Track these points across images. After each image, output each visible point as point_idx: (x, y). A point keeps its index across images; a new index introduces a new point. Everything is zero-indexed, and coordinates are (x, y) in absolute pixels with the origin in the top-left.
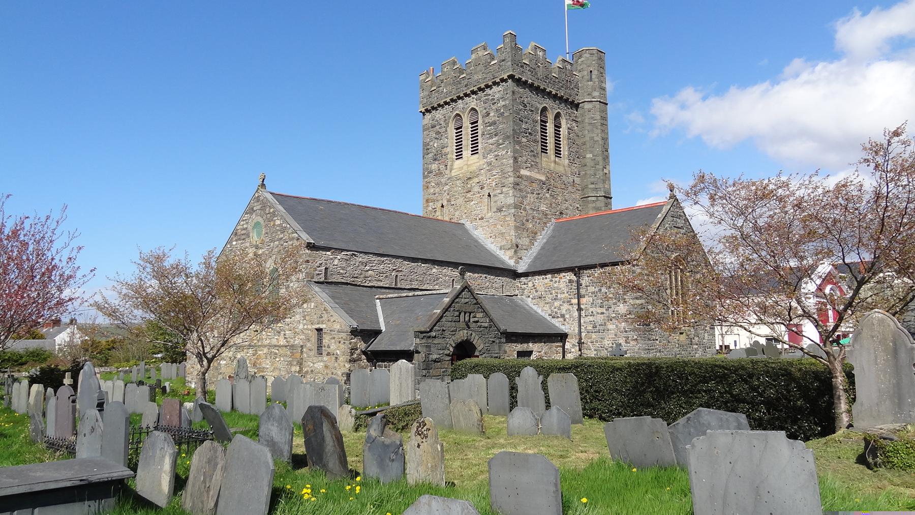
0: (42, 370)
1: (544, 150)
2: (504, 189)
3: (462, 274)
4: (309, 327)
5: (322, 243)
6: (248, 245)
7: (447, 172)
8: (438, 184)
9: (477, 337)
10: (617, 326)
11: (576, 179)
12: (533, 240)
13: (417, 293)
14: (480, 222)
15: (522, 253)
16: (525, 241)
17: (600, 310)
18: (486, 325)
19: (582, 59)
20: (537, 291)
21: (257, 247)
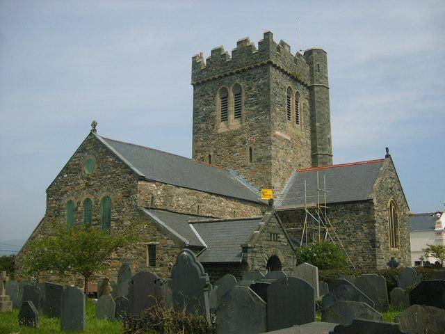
0: (437, 262)
4: (142, 243)
5: (148, 177)
6: (79, 177)
8: (205, 140)
13: (215, 220)
18: (286, 244)
21: (88, 179)
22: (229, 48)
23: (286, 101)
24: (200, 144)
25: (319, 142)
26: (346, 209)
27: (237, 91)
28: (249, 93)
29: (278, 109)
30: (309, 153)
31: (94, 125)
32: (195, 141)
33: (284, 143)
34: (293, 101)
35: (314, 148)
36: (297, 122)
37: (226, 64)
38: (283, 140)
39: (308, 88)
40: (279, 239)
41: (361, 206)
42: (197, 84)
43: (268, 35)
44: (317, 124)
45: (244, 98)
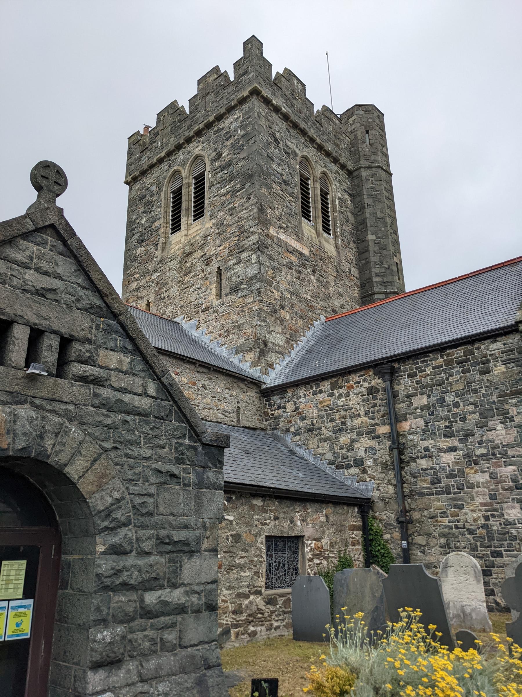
1: (306, 214)
2: (244, 256)
3: (107, 296)
7: (158, 253)
9: (90, 450)
10: (493, 476)
11: (352, 269)
12: (293, 338)
14: (202, 316)
15: (271, 357)
16: (277, 339)
17: (445, 443)
18: (145, 403)
19: (353, 118)
20: (303, 419)
24: (134, 285)
26: (448, 363)
39: (350, 173)
43: (253, 45)
44: (371, 237)
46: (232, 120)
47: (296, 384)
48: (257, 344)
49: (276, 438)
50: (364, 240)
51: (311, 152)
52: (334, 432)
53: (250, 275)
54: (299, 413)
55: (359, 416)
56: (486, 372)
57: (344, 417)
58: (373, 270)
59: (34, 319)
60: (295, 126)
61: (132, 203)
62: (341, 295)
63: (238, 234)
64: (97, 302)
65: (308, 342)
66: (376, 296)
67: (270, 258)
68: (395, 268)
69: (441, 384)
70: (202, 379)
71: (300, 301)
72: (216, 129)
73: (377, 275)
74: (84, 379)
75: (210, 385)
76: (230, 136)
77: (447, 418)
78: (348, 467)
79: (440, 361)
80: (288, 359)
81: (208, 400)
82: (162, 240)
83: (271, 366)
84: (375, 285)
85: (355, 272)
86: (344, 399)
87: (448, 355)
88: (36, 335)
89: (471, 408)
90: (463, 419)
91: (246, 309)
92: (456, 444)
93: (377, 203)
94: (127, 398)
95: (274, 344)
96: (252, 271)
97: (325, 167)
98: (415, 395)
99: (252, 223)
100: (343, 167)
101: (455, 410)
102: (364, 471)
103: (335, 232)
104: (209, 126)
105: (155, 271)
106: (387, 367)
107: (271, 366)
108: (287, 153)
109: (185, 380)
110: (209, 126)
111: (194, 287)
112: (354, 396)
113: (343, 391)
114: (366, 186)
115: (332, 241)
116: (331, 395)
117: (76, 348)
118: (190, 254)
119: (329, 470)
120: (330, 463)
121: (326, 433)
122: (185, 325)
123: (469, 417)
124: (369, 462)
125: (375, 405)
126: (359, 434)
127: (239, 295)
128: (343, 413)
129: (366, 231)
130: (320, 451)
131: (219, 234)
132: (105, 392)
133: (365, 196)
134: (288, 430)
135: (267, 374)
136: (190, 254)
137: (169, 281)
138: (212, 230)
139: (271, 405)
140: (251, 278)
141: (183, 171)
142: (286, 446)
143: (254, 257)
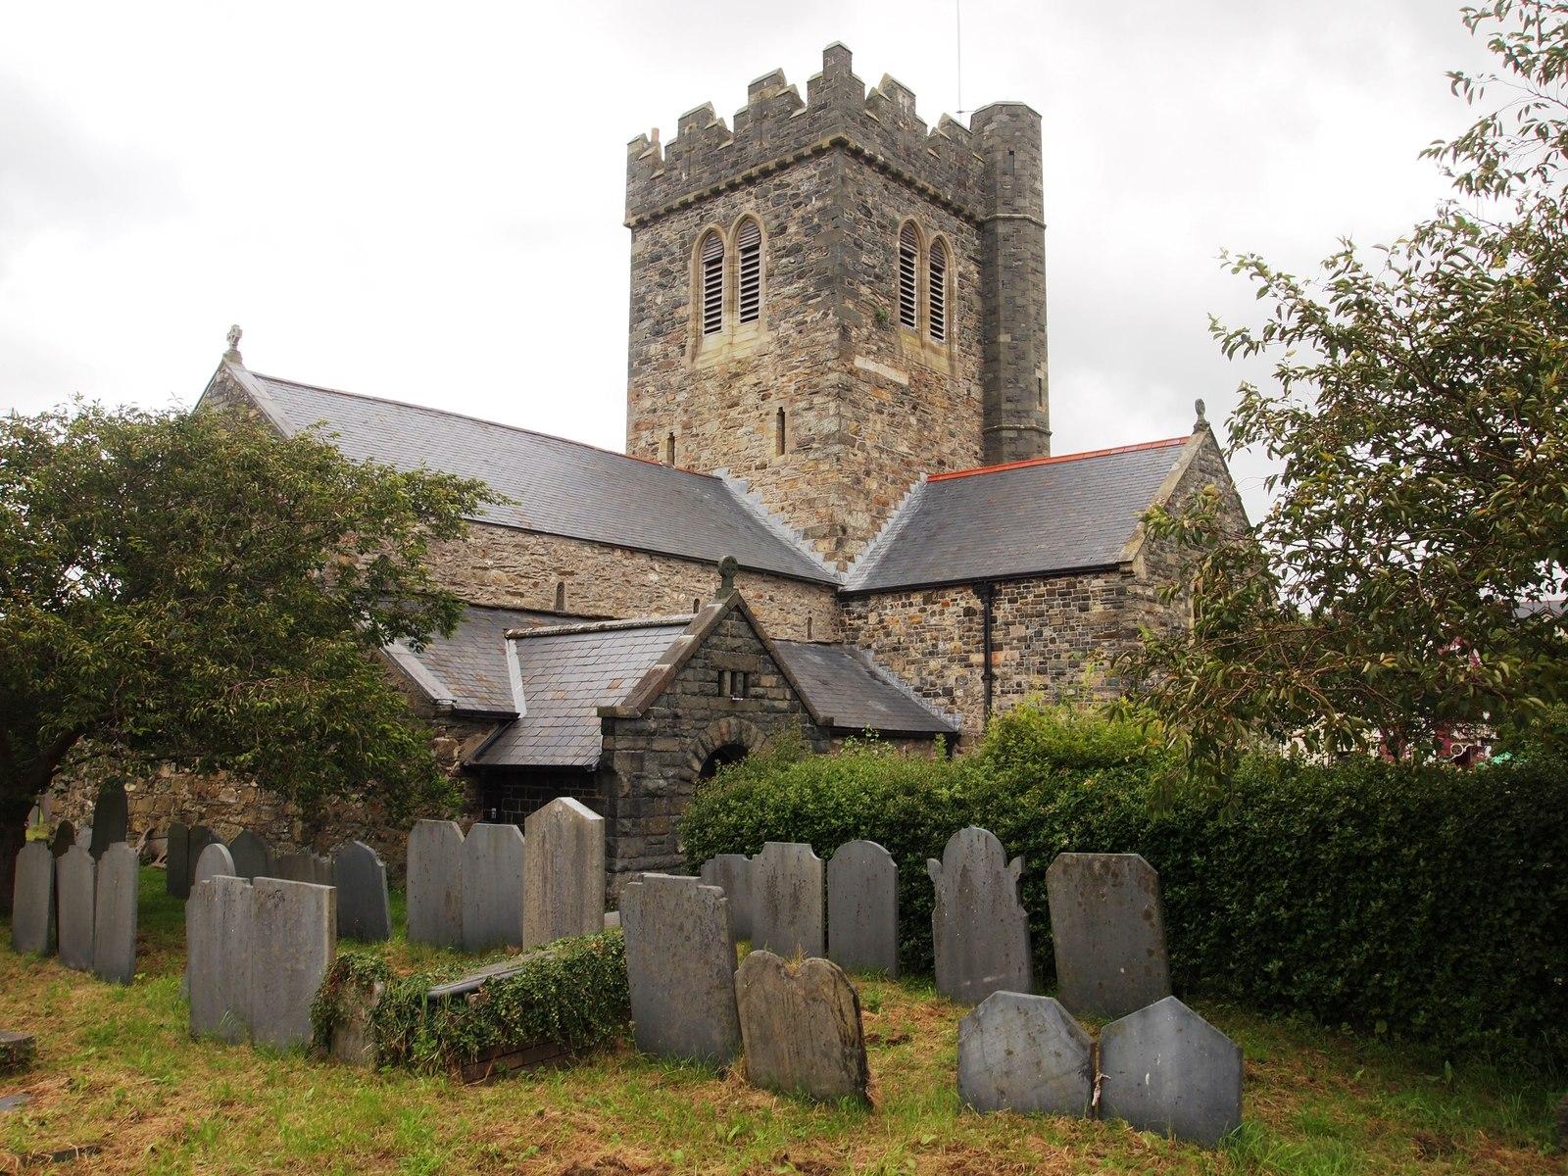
1: (907, 316)
2: (817, 400)
7: (686, 360)
11: (974, 389)
14: (757, 475)
15: (851, 547)
16: (859, 520)
17: (1037, 680)
18: (784, 705)
20: (888, 635)
22: (729, 104)
23: (896, 266)
24: (647, 403)
25: (1008, 391)
26: (1051, 593)
27: (749, 240)
28: (780, 242)
29: (865, 290)
30: (974, 426)
31: (235, 337)
32: (635, 395)
33: (886, 396)
34: (922, 272)
35: (990, 412)
36: (936, 330)
37: (719, 158)
38: (880, 384)
39: (980, 226)
40: (753, 691)
41: (1098, 583)
42: (643, 219)
43: (837, 56)
44: (1004, 338)
45: (764, 259)
46: (803, 176)
47: (883, 592)
48: (832, 533)
49: (853, 653)
50: (994, 342)
51: (918, 212)
52: (924, 654)
53: (825, 432)
54: (884, 628)
55: (952, 639)
56: (1084, 609)
57: (936, 639)
58: (1003, 391)
59: (731, 667)
60: (897, 177)
61: (638, 263)
62: (952, 435)
63: (809, 364)
64: (759, 646)
65: (901, 517)
66: (1004, 434)
67: (854, 403)
68: (1035, 389)
69: (1040, 615)
70: (768, 589)
71: (892, 459)
72: (777, 181)
73: (1009, 400)
74: (756, 697)
75: (778, 595)
76: (800, 203)
77: (1042, 654)
78: (937, 695)
79: (1043, 589)
80: (873, 545)
81: (776, 614)
82: (690, 342)
83: (851, 559)
84: (1004, 415)
85: (977, 392)
86: (937, 617)
87: (1051, 584)
88: (734, 674)
89: (1066, 646)
90: (1058, 657)
91: (819, 477)
92: (1048, 682)
93: (1017, 280)
94: (776, 703)
95: (855, 528)
96: (830, 426)
97: (941, 227)
98: (1014, 623)
99: (832, 355)
100: (969, 219)
101: (1051, 646)
102: (953, 702)
103: (950, 334)
104: (766, 174)
105: (681, 389)
106: (987, 588)
107: (851, 559)
108: (883, 227)
109: (751, 594)
110: (766, 174)
111: (743, 430)
112: (951, 614)
113: (936, 607)
114: (1002, 251)
115: (945, 349)
116: (923, 610)
117: (752, 678)
118: (737, 375)
119: (915, 697)
120: (917, 689)
121: (914, 655)
122: (731, 483)
123: (1063, 655)
124: (959, 693)
125: (970, 630)
126: (951, 660)
127: (811, 457)
128: (935, 634)
129: (997, 327)
130: (906, 674)
131: (783, 357)
132: (766, 702)
133: (1000, 269)
134: (869, 647)
135: (845, 570)
136: (737, 375)
137: (704, 410)
138: (771, 348)
139: (849, 613)
140: (827, 437)
141: (724, 235)
142: (866, 667)
143: (832, 405)
